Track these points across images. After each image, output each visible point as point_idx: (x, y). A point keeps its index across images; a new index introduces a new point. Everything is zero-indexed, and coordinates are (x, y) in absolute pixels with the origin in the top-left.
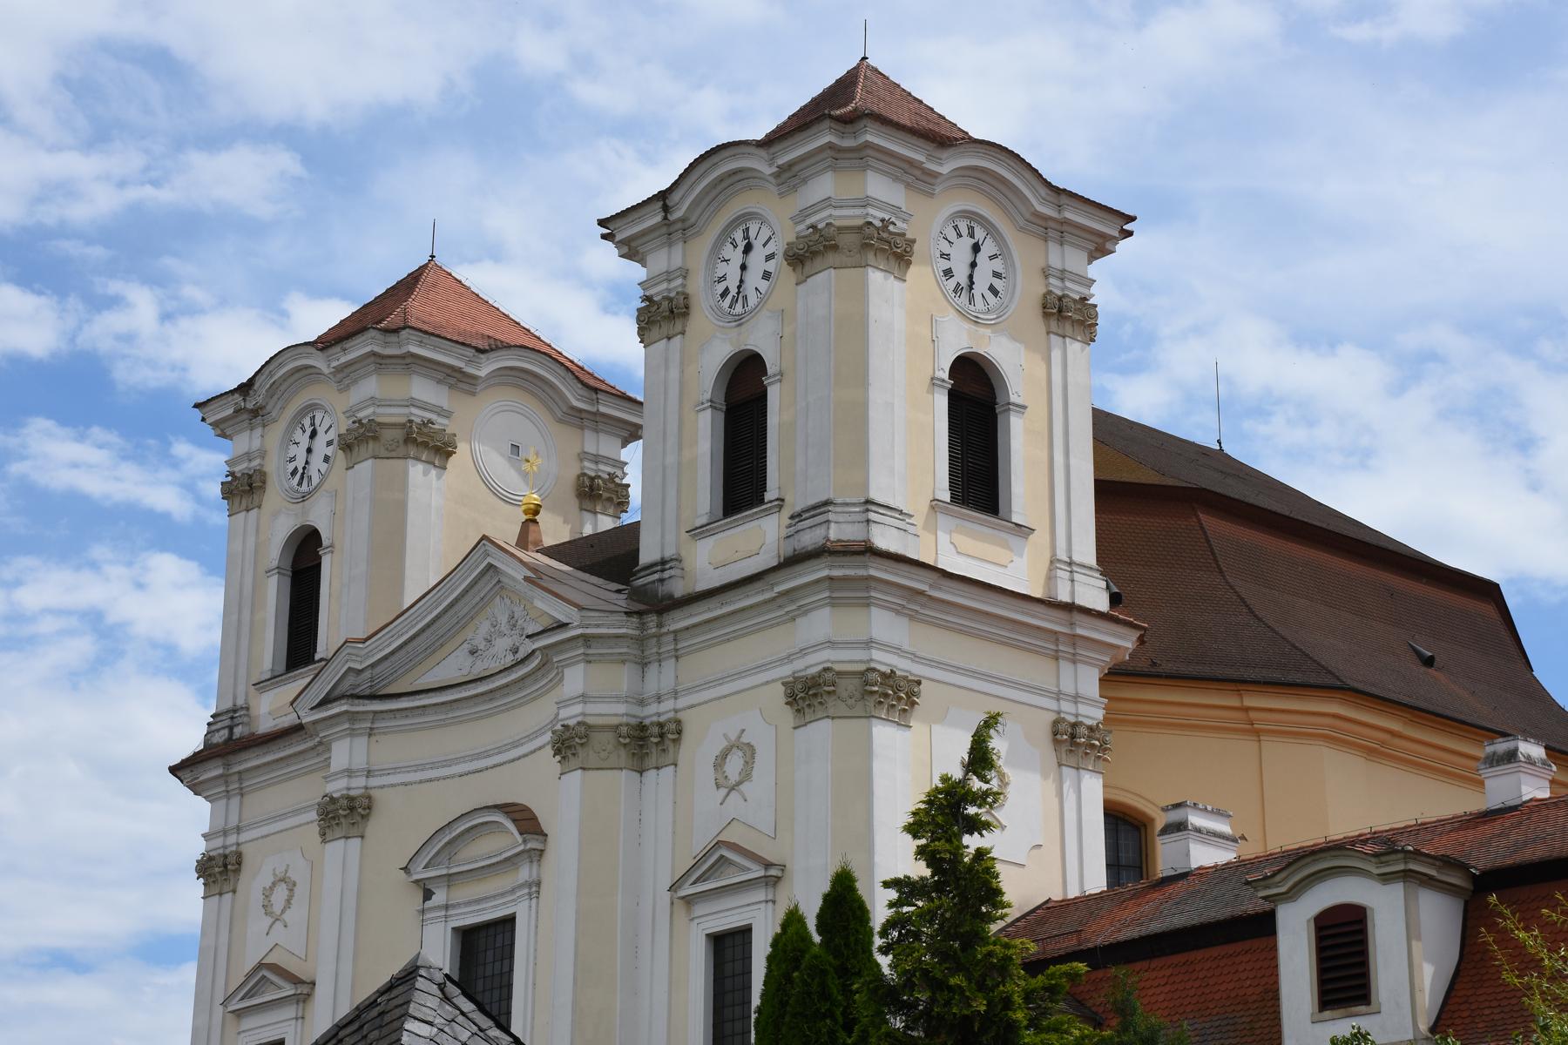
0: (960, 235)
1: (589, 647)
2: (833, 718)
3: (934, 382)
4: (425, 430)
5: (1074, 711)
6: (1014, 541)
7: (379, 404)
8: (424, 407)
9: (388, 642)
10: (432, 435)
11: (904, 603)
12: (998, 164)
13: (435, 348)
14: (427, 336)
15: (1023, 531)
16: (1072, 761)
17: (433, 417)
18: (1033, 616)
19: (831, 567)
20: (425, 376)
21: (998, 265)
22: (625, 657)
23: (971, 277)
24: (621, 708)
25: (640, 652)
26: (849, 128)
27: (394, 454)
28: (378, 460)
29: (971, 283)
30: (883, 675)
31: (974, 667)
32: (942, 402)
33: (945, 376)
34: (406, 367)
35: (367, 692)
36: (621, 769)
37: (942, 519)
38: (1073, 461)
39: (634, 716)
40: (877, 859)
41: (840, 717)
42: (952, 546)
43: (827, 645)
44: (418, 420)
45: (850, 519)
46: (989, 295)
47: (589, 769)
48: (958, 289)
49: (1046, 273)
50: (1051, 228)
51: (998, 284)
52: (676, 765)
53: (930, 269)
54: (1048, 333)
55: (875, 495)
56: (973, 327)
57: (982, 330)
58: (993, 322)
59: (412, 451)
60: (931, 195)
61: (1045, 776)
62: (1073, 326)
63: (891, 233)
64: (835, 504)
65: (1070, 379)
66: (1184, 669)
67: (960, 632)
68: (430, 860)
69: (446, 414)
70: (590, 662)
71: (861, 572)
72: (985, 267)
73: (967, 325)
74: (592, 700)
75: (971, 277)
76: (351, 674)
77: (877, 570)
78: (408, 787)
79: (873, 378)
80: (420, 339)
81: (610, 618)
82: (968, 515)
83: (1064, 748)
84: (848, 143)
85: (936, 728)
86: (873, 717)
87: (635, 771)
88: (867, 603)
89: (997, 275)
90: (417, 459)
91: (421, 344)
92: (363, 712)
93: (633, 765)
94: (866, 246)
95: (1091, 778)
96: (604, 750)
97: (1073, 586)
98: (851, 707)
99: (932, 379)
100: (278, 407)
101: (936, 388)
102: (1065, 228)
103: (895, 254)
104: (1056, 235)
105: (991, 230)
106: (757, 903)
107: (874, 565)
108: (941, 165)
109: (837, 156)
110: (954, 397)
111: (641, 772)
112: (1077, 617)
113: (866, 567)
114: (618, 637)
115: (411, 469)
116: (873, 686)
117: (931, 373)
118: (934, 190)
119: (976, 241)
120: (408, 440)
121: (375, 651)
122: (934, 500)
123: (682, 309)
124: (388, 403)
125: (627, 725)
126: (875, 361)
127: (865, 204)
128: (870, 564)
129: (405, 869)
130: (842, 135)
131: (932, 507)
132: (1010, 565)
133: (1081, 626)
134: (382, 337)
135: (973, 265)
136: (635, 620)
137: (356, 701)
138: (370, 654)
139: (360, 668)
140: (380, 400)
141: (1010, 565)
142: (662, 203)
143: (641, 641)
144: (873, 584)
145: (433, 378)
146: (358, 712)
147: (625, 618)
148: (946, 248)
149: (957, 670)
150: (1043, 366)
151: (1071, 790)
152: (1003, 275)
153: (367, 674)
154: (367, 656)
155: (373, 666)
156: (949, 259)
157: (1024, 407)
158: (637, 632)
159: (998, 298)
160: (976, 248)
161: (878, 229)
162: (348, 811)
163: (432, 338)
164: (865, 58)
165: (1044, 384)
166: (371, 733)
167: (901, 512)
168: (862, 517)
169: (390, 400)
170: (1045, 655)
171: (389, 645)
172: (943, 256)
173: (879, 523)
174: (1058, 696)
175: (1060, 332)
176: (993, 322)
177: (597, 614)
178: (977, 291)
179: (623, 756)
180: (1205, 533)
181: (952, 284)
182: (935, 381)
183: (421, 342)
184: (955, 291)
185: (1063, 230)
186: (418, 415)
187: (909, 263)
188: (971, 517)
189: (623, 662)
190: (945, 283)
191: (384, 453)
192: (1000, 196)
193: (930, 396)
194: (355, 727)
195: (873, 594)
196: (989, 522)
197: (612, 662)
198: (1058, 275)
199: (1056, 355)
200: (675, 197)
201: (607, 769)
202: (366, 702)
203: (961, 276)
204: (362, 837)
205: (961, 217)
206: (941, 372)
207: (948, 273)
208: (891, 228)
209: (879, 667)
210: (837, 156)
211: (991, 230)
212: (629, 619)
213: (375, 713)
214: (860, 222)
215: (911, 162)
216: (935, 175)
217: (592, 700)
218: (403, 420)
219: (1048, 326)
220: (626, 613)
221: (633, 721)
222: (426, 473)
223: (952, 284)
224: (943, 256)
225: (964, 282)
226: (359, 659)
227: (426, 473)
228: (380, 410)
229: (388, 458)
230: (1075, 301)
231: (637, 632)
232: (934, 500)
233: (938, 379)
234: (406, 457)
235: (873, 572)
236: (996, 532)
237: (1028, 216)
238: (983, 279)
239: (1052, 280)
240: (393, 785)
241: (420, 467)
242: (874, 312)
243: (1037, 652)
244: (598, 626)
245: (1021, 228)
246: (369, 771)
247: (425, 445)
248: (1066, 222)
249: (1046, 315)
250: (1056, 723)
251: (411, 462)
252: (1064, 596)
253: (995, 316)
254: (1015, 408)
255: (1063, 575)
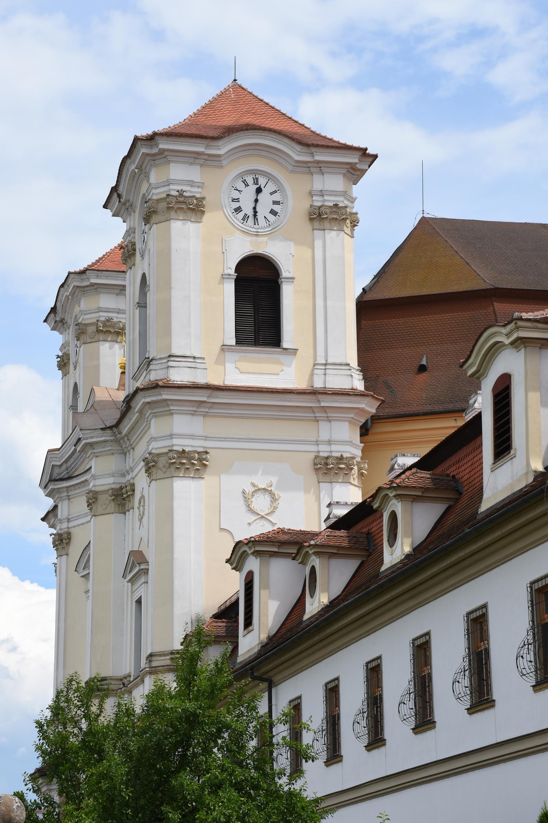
0: (247, 185)
1: (94, 449)
2: (156, 480)
3: (224, 277)
4: (109, 324)
5: (329, 450)
6: (283, 358)
7: (85, 313)
8: (108, 310)
9: (69, 449)
10: (114, 325)
11: (195, 409)
12: (265, 139)
13: (107, 277)
14: (100, 272)
15: (294, 351)
16: (327, 478)
17: (110, 315)
18: (290, 401)
19: (145, 397)
20: (104, 293)
21: (277, 197)
22: (112, 452)
23: (255, 208)
24: (111, 480)
25: (120, 448)
26: (153, 142)
27: (93, 340)
28: (86, 344)
29: (255, 212)
30: (178, 452)
31: (252, 437)
32: (230, 288)
33: (232, 271)
34: (96, 290)
35: (66, 476)
36: (113, 513)
37: (228, 355)
38: (329, 303)
39: (118, 483)
40: (176, 555)
41: (159, 479)
42: (236, 370)
43: (151, 440)
44: (103, 319)
45: (162, 367)
46: (271, 217)
47: (97, 515)
48: (245, 218)
49: (311, 194)
50: (312, 167)
51: (276, 208)
52: (133, 508)
53: (222, 212)
54: (313, 230)
55: (175, 351)
56: (254, 238)
57: (260, 239)
58: (269, 232)
59: (101, 336)
60: (222, 167)
61: (307, 491)
62: (330, 222)
63: (185, 197)
64: (156, 359)
65: (328, 254)
66: (437, 408)
67: (243, 417)
68: (85, 565)
69: (201, 185)
70: (97, 456)
71: (159, 398)
72: (265, 199)
73: (248, 239)
74: (98, 477)
75: (255, 208)
76: (56, 468)
77: (166, 395)
78: (84, 525)
79: (174, 283)
80: (97, 275)
81: (96, 433)
82: (246, 350)
83: (321, 472)
84: (155, 151)
85: (223, 477)
86: (173, 477)
87: (122, 513)
88: (171, 413)
89: (276, 203)
90: (105, 340)
91: (98, 277)
92: (62, 488)
93: (119, 511)
94: (169, 208)
95: (341, 486)
96: (105, 504)
97: (325, 377)
98: (164, 473)
99: (222, 275)
100: (69, 317)
101: (225, 280)
102: (320, 165)
103: (193, 210)
104: (317, 170)
105: (270, 177)
106: (141, 585)
107: (165, 393)
108: (219, 149)
109: (154, 158)
110: (238, 282)
111: (125, 513)
112: (320, 397)
113: (161, 394)
114: (105, 441)
115: (101, 347)
116: (172, 459)
117: (222, 271)
118: (222, 164)
119: (258, 186)
120: (98, 331)
121: (65, 454)
122: (223, 345)
123: (131, 251)
124: (89, 312)
125: (112, 489)
126: (176, 274)
127: (168, 184)
128: (162, 393)
129: (76, 571)
130: (152, 147)
131: (222, 350)
132: (281, 373)
133: (323, 401)
134: (79, 277)
135: (256, 201)
136: (108, 431)
137: (56, 483)
138: (63, 456)
139: (59, 464)
140: (86, 311)
141: (281, 373)
142: (116, 193)
143: (117, 441)
144: (169, 403)
145: (113, 293)
146: (59, 488)
147: (101, 432)
148: (236, 195)
149: (239, 440)
150: (310, 251)
151: (326, 496)
152: (281, 202)
153: (64, 467)
154: (62, 457)
155: (66, 461)
156: (239, 202)
157: (293, 278)
158: (112, 438)
159: (277, 216)
160: (259, 191)
161: (176, 197)
162: (59, 542)
163: (103, 272)
164: (235, 80)
165: (310, 261)
166: (69, 498)
167: (194, 358)
168: (165, 366)
169: (90, 310)
170: (310, 420)
171: (70, 450)
172: (233, 200)
173: (173, 367)
174: (317, 443)
175: (321, 227)
176: (269, 232)
177: (89, 431)
178: (260, 216)
179: (112, 507)
180: (496, 315)
181: (241, 215)
182: (224, 276)
183: (97, 276)
184: (243, 219)
185: (320, 166)
186: (103, 316)
187: (203, 212)
188: (250, 350)
189: (113, 454)
190: (236, 216)
191: (89, 340)
192: (276, 158)
193: (222, 286)
194: (61, 496)
195: (171, 408)
196: (264, 351)
197: (107, 455)
198: (319, 194)
199: (318, 244)
200: (121, 189)
201: (106, 514)
202: (61, 482)
203: (248, 210)
204: (67, 555)
205: (246, 174)
206: (229, 270)
207: (238, 210)
208: (185, 194)
209: (175, 448)
210: (154, 158)
211: (270, 177)
212: (105, 432)
213: (67, 487)
214: (164, 195)
215: (198, 153)
216: (219, 156)
217: (98, 477)
218: (94, 321)
219: (313, 226)
220: (101, 429)
221: (117, 486)
222: (111, 348)
223: (241, 215)
224: (233, 200)
225: (250, 213)
226: (58, 459)
227: (111, 348)
228: (86, 317)
229: (90, 343)
230: (330, 207)
231: (112, 438)
232: (223, 345)
233: (225, 275)
234: (99, 341)
235: (165, 397)
236: (271, 356)
237: (293, 163)
238: (263, 210)
239: (315, 198)
240: (78, 525)
241: (107, 345)
242: (174, 245)
243: (302, 420)
244: (92, 438)
245: (291, 171)
246: (68, 519)
247: (109, 332)
248: (318, 162)
249: (311, 220)
250: (316, 457)
251: (101, 343)
252: (318, 384)
253: (270, 229)
254: (286, 280)
255: (319, 372)
